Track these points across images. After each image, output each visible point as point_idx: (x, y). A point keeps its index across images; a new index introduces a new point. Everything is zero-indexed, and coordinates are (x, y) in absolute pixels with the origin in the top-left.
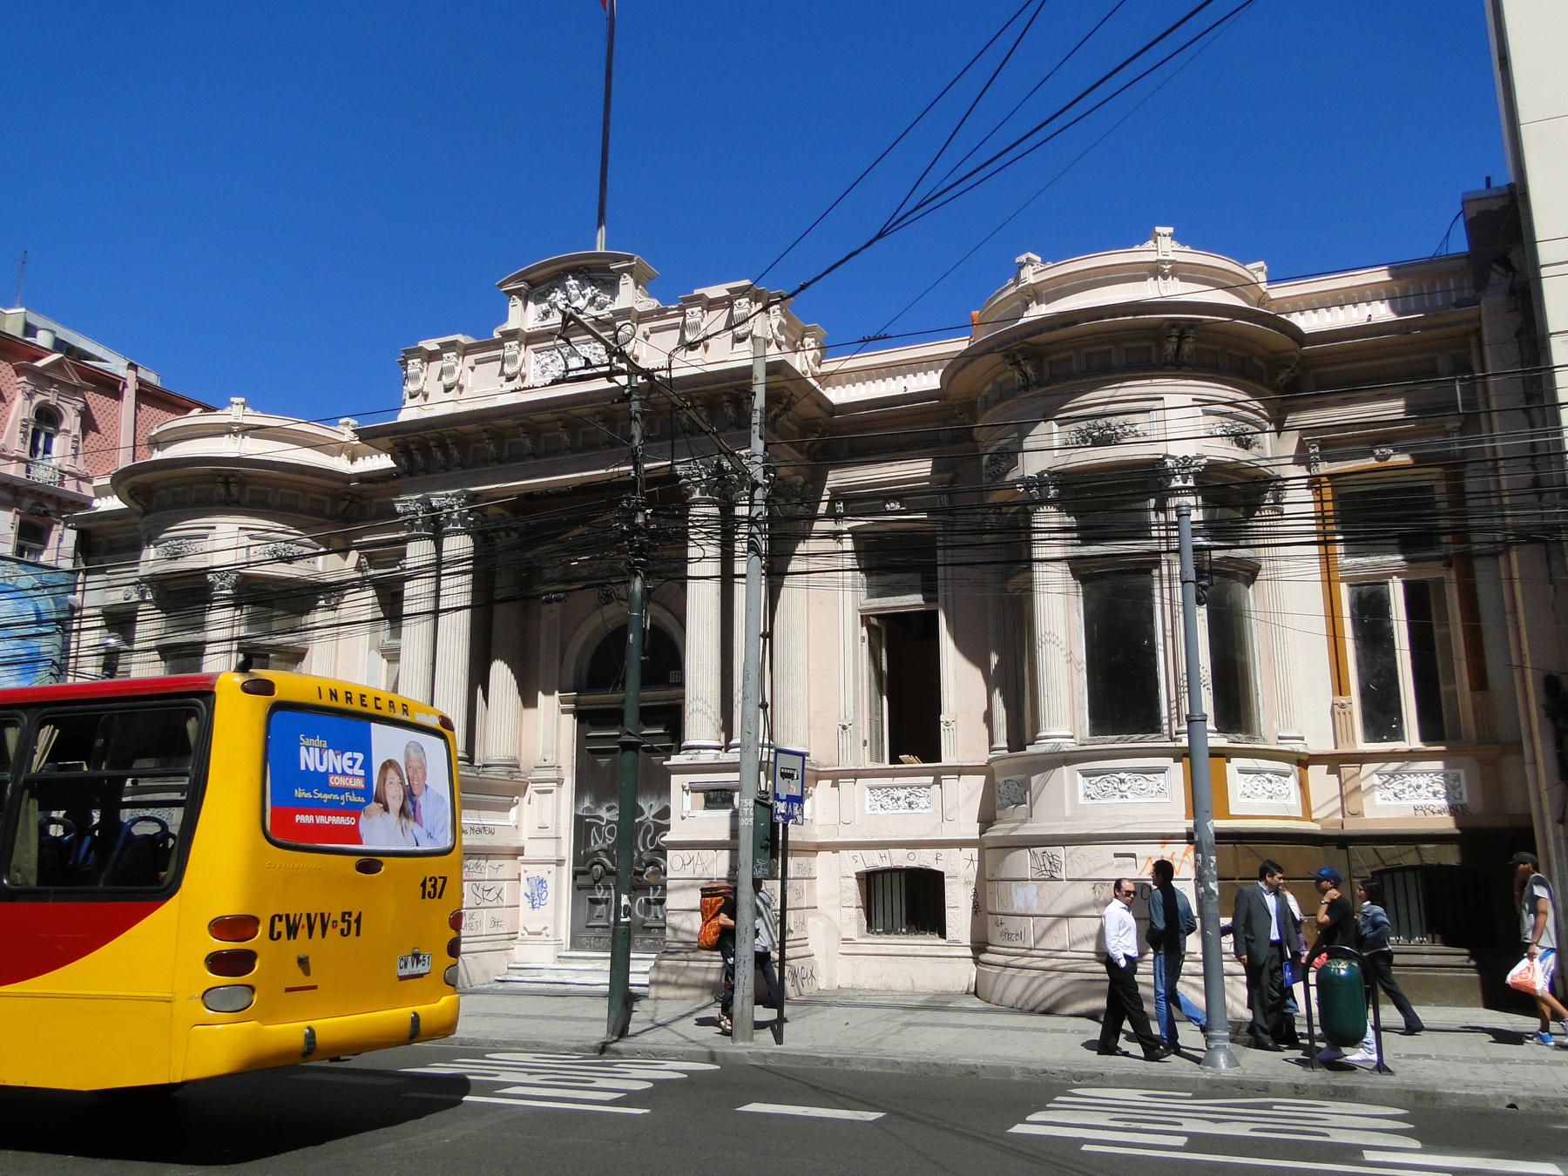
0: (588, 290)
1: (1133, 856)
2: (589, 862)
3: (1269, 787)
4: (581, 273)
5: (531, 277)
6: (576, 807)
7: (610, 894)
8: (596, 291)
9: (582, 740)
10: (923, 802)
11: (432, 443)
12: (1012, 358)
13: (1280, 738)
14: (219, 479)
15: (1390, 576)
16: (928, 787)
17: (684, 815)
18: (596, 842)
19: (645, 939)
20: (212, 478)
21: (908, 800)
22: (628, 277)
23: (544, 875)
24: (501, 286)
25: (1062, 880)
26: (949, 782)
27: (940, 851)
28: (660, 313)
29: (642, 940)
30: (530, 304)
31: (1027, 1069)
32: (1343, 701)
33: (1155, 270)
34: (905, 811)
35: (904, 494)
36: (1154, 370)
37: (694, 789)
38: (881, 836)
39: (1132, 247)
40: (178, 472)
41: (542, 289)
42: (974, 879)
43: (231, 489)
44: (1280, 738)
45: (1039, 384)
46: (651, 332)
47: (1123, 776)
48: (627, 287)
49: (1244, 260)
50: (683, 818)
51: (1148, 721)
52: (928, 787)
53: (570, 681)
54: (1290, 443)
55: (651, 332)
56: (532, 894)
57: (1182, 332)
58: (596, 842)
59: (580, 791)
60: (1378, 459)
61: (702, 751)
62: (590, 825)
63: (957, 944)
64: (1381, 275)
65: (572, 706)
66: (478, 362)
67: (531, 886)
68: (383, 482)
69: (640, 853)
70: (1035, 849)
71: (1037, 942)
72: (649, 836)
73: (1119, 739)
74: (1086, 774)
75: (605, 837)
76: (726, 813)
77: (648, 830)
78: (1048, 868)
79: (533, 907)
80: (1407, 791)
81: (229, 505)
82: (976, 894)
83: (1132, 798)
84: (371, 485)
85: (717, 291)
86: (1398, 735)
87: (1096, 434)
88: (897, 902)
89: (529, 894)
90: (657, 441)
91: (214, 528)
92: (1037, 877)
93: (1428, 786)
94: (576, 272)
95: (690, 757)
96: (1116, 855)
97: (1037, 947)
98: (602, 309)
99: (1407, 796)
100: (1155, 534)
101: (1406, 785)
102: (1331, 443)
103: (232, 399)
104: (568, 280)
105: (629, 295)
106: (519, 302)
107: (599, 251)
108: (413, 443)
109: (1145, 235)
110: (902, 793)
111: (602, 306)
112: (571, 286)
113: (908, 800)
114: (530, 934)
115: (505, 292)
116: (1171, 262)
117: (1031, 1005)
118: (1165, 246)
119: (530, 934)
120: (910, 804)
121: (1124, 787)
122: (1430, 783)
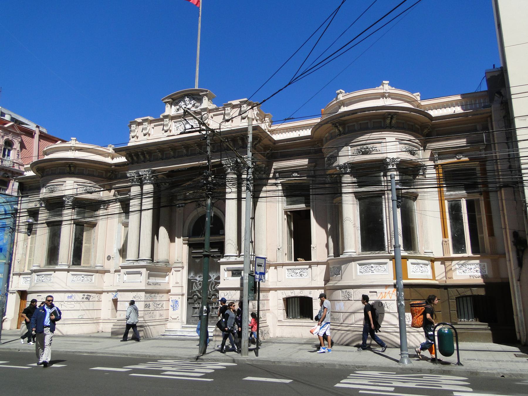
0: (192, 102)
2: (193, 295)
4: (190, 96)
8: (195, 102)
9: (190, 253)
10: (305, 274)
12: (335, 125)
13: (96, 266)
14: (67, 165)
17: (225, 279)
18: (195, 288)
21: (300, 273)
22: (206, 97)
23: (177, 299)
24: (163, 100)
25: (352, 300)
26: (314, 267)
28: (217, 110)
32: (446, 240)
33: (383, 96)
36: (383, 129)
37: (228, 270)
40: (53, 163)
41: (177, 101)
45: (344, 134)
46: (214, 116)
47: (372, 265)
49: (413, 92)
50: (224, 280)
55: (214, 116)
56: (174, 305)
57: (392, 116)
58: (195, 288)
59: (189, 271)
62: (193, 282)
66: (155, 126)
69: (210, 292)
71: (343, 321)
72: (213, 286)
73: (371, 253)
75: (198, 286)
77: (213, 284)
79: (174, 310)
85: (236, 102)
91: (65, 182)
92: (344, 299)
93: (474, 268)
94: (188, 95)
95: (227, 259)
98: (197, 108)
99: (467, 272)
100: (383, 184)
103: (72, 138)
104: (185, 98)
105: (206, 103)
106: (169, 106)
109: (380, 84)
110: (298, 271)
111: (197, 107)
112: (186, 100)
113: (300, 273)
114: (173, 319)
115: (164, 102)
116: (388, 93)
119: (173, 319)
121: (373, 269)
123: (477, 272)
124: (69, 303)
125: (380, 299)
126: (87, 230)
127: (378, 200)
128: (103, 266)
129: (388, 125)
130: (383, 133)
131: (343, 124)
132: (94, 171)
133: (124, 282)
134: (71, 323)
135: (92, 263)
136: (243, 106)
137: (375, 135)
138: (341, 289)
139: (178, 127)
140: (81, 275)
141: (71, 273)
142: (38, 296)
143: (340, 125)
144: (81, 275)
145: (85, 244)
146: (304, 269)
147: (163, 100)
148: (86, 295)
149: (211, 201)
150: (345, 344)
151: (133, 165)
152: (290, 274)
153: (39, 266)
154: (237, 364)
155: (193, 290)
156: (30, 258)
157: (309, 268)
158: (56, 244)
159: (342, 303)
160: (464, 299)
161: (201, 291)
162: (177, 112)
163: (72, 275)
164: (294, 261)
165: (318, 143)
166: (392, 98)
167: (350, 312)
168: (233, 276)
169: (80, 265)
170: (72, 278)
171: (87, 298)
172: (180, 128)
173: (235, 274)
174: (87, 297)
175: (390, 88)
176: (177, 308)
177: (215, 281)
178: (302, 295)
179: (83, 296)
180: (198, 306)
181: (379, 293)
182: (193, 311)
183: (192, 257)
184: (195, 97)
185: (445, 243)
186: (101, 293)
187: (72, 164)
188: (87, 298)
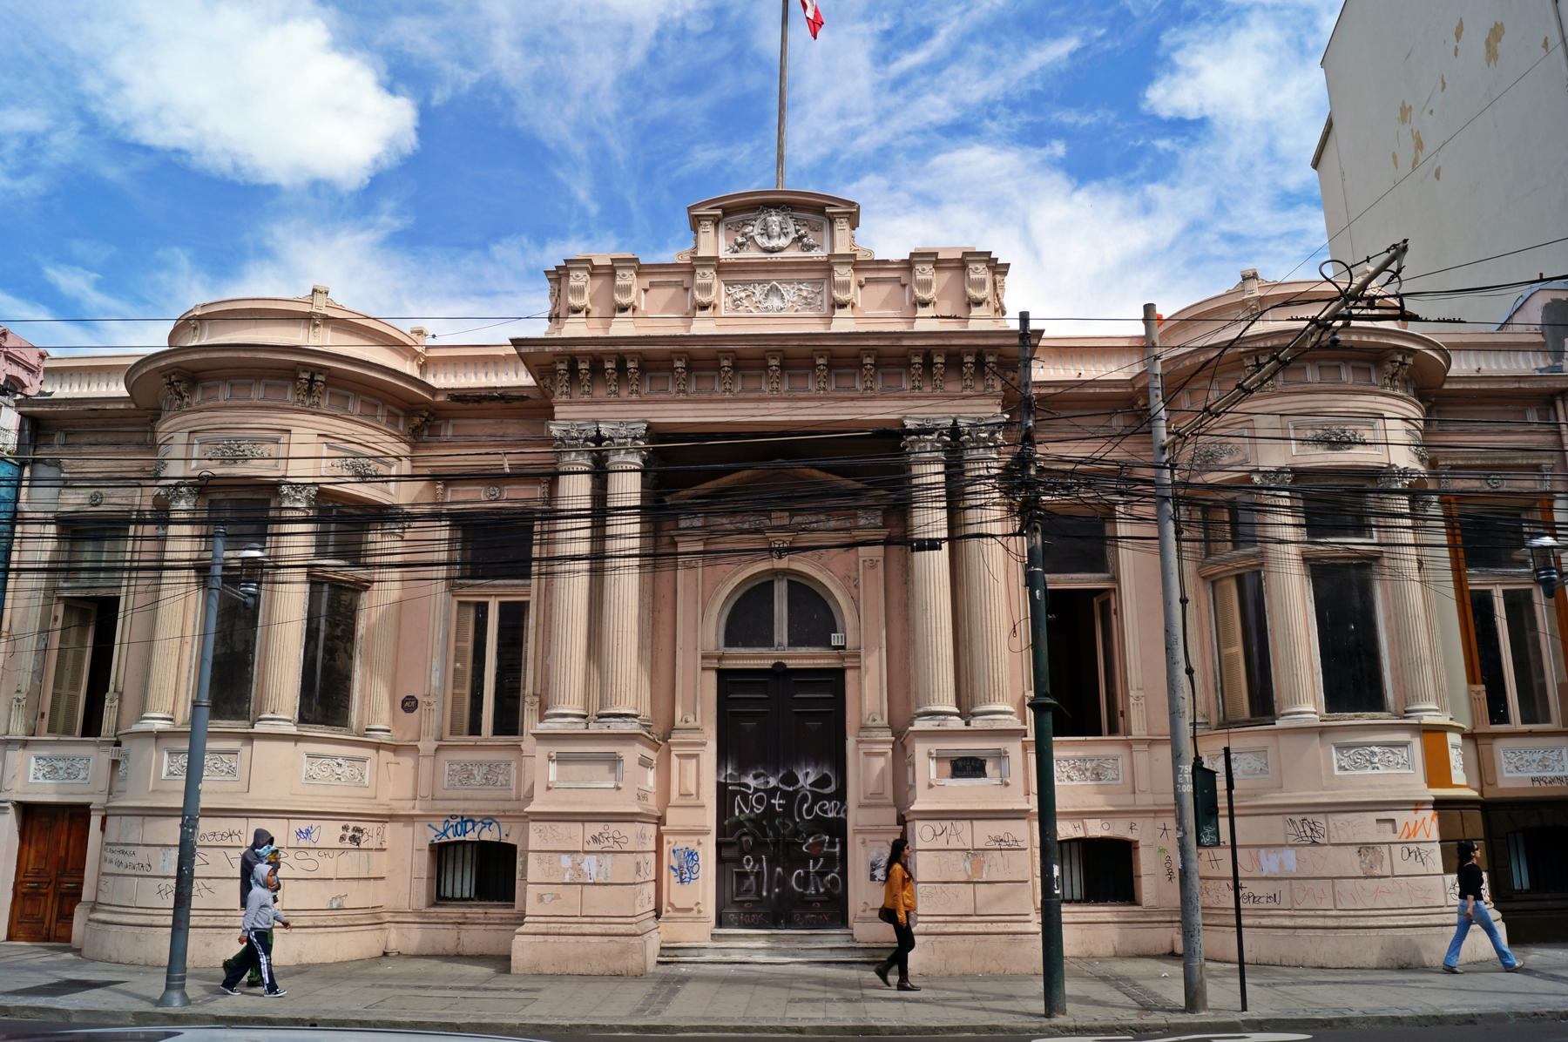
1: (1392, 821)
2: (737, 834)
6: (718, 774)
7: (761, 867)
13: (367, 730)
18: (741, 811)
19: (806, 914)
23: (693, 846)
29: (802, 915)
31: (1519, 1013)
44: (367, 730)
51: (1375, 701)
56: (681, 867)
58: (741, 811)
61: (950, 718)
62: (735, 793)
67: (679, 858)
68: (475, 401)
69: (796, 823)
72: (805, 806)
74: (1340, 748)
75: (752, 807)
77: (805, 798)
78: (1309, 833)
79: (682, 881)
83: (1382, 771)
84: (459, 404)
86: (1547, 720)
88: (463, 881)
89: (676, 867)
91: (289, 431)
92: (1296, 842)
95: (937, 723)
98: (808, 250)
106: (711, 229)
114: (678, 910)
119: (678, 910)
124: (301, 855)
134: (311, 924)
140: (336, 758)
148: (351, 828)
149: (1043, 539)
153: (171, 720)
154: (1310, 1037)
158: (239, 647)
160: (458, 895)
161: (765, 823)
162: (736, 252)
164: (1524, 721)
171: (353, 839)
174: (354, 836)
176: (693, 876)
177: (811, 792)
179: (342, 832)
180: (753, 867)
182: (740, 884)
188: (353, 839)
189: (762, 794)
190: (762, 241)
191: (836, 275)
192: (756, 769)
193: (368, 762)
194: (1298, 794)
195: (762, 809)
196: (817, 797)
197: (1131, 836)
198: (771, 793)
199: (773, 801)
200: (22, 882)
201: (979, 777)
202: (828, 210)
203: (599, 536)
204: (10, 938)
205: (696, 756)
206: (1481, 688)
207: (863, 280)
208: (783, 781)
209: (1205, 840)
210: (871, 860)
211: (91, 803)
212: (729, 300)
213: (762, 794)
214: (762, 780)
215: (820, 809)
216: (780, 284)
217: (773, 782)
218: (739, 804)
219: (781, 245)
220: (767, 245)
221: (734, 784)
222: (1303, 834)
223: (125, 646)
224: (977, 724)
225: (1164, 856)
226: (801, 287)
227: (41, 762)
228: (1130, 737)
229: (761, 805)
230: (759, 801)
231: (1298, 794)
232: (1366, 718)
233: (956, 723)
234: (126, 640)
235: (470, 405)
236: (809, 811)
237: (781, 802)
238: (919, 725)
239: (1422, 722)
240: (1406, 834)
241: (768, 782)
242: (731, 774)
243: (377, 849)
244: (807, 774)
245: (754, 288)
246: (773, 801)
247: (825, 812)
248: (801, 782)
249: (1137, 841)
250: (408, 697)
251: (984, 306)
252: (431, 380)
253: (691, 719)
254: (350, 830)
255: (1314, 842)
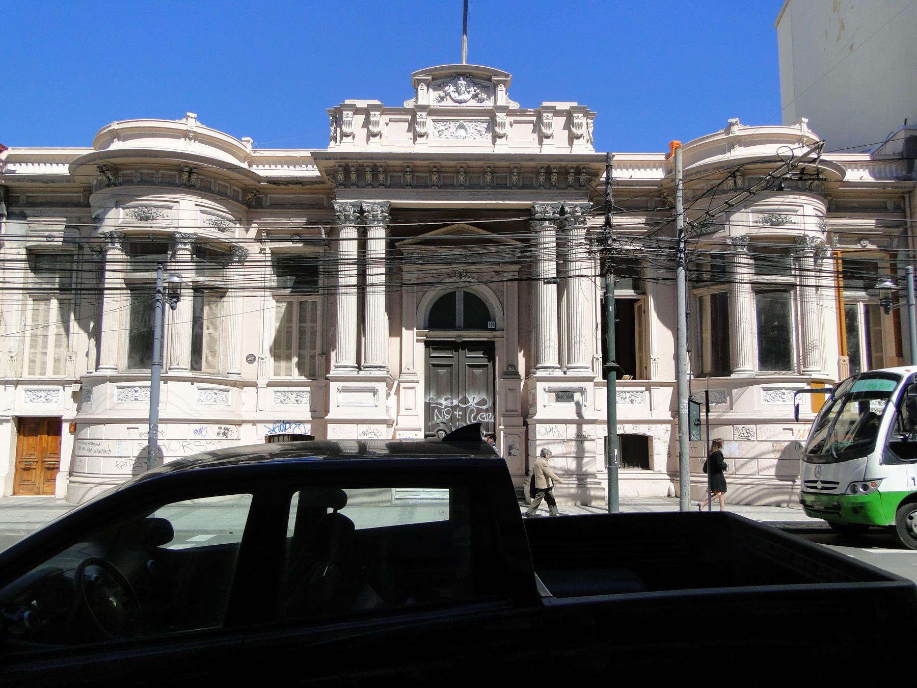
0: (472, 89)
1: (792, 429)
2: (436, 430)
3: (215, 396)
4: (467, 77)
5: (434, 73)
8: (478, 91)
9: (428, 357)
10: (638, 400)
11: (353, 169)
12: (102, 169)
13: (228, 373)
14: (408, 169)
15: (859, 301)
16: (642, 392)
17: (339, 405)
18: (438, 418)
20: (180, 169)
21: (46, 398)
22: (503, 86)
24: (415, 75)
25: (754, 441)
26: (655, 391)
27: (650, 425)
28: (522, 112)
30: (431, 90)
32: (845, 359)
33: (185, 135)
34: (629, 405)
35: (861, 236)
36: (800, 191)
37: (550, 391)
38: (222, 417)
39: (790, 126)
40: (159, 160)
41: (439, 82)
42: (668, 439)
43: (192, 177)
44: (228, 373)
45: (115, 185)
46: (514, 123)
47: (784, 391)
48: (501, 92)
49: (239, 138)
50: (545, 406)
52: (642, 392)
53: (422, 324)
54: (252, 233)
55: (390, 121)
57: (191, 169)
59: (428, 387)
60: (862, 246)
61: (555, 370)
62: (434, 408)
63: (660, 472)
64: (866, 157)
65: (424, 338)
66: (391, 120)
70: (737, 426)
71: (736, 470)
72: (473, 415)
73: (775, 373)
75: (444, 416)
76: (572, 405)
77: (472, 411)
78: (746, 435)
80: (36, 398)
81: (189, 187)
82: (669, 448)
85: (361, 104)
87: (774, 220)
90: (416, 188)
91: (178, 202)
92: (738, 439)
93: (630, 397)
94: (465, 75)
95: (549, 372)
96: (784, 429)
97: (737, 473)
98: (481, 102)
99: (36, 401)
100: (793, 272)
101: (286, 397)
102: (844, 235)
103: (189, 114)
104: (460, 80)
105: (503, 97)
106: (425, 88)
107: (464, 64)
108: (381, 167)
109: (182, 115)
110: (43, 394)
111: (481, 101)
112: (462, 85)
113: (46, 398)
115: (416, 79)
116: (194, 132)
117: (738, 500)
118: (191, 123)
120: (632, 401)
121: (784, 396)
122: (46, 395)
123: (880, 404)
125: (797, 439)
126: (210, 303)
127: (785, 295)
128: (240, 374)
129: (542, 183)
130: (801, 197)
131: (116, 169)
132: (227, 187)
133: (338, 406)
135: (220, 367)
136: (578, 117)
137: (793, 199)
138: (733, 425)
139: (442, 130)
140: (214, 389)
141: (197, 385)
142: (128, 428)
143: (108, 170)
144: (214, 389)
145: (207, 329)
146: (637, 392)
147: (415, 75)
148: (223, 428)
150: (744, 502)
151: (347, 189)
152: (280, 400)
153: (116, 369)
155: (434, 422)
156: (58, 350)
157: (645, 391)
159: (736, 444)
161: (451, 424)
162: (439, 102)
163: (199, 389)
165: (668, 196)
166: (200, 142)
167: (749, 457)
168: (559, 401)
169: (201, 370)
170: (199, 395)
171: (224, 434)
172: (445, 132)
173: (562, 397)
174: (225, 432)
175: (198, 124)
178: (637, 432)
181: (796, 430)
183: (432, 364)
184: (477, 81)
185: (11, 359)
186: (239, 423)
187: (195, 168)
188: (224, 434)
189: (449, 409)
190: (455, 95)
191: (497, 118)
192: (446, 395)
193: (230, 392)
194: (741, 414)
195: (449, 416)
196: (479, 411)
197: (648, 433)
198: (454, 408)
199: (455, 413)
200: (20, 462)
201: (570, 402)
202: (494, 78)
203: (362, 275)
204: (14, 494)
205: (413, 388)
206: (846, 358)
207: (513, 121)
208: (460, 402)
209: (692, 438)
210: (509, 444)
211: (62, 416)
212: (436, 131)
213: (449, 409)
214: (449, 401)
215: (481, 417)
216: (464, 122)
217: (455, 402)
218: (436, 414)
219: (465, 99)
220: (458, 98)
221: (434, 403)
222: (743, 435)
223: (170, 326)
224: (570, 373)
225: (29, 181)
226: (476, 124)
227: (28, 393)
228: (650, 381)
229: (449, 415)
230: (448, 412)
231: (741, 414)
232: (781, 375)
233: (559, 373)
234: (170, 323)
235: (282, 186)
236: (475, 418)
237: (461, 413)
238: (540, 374)
239: (811, 377)
240: (798, 437)
241: (452, 402)
242: (432, 398)
243: (236, 440)
244: (474, 398)
245: (450, 124)
246: (455, 413)
247: (483, 419)
248: (471, 403)
249: (652, 436)
250: (249, 355)
251: (581, 139)
252: (254, 169)
253: (411, 368)
254: (223, 429)
255: (748, 439)
